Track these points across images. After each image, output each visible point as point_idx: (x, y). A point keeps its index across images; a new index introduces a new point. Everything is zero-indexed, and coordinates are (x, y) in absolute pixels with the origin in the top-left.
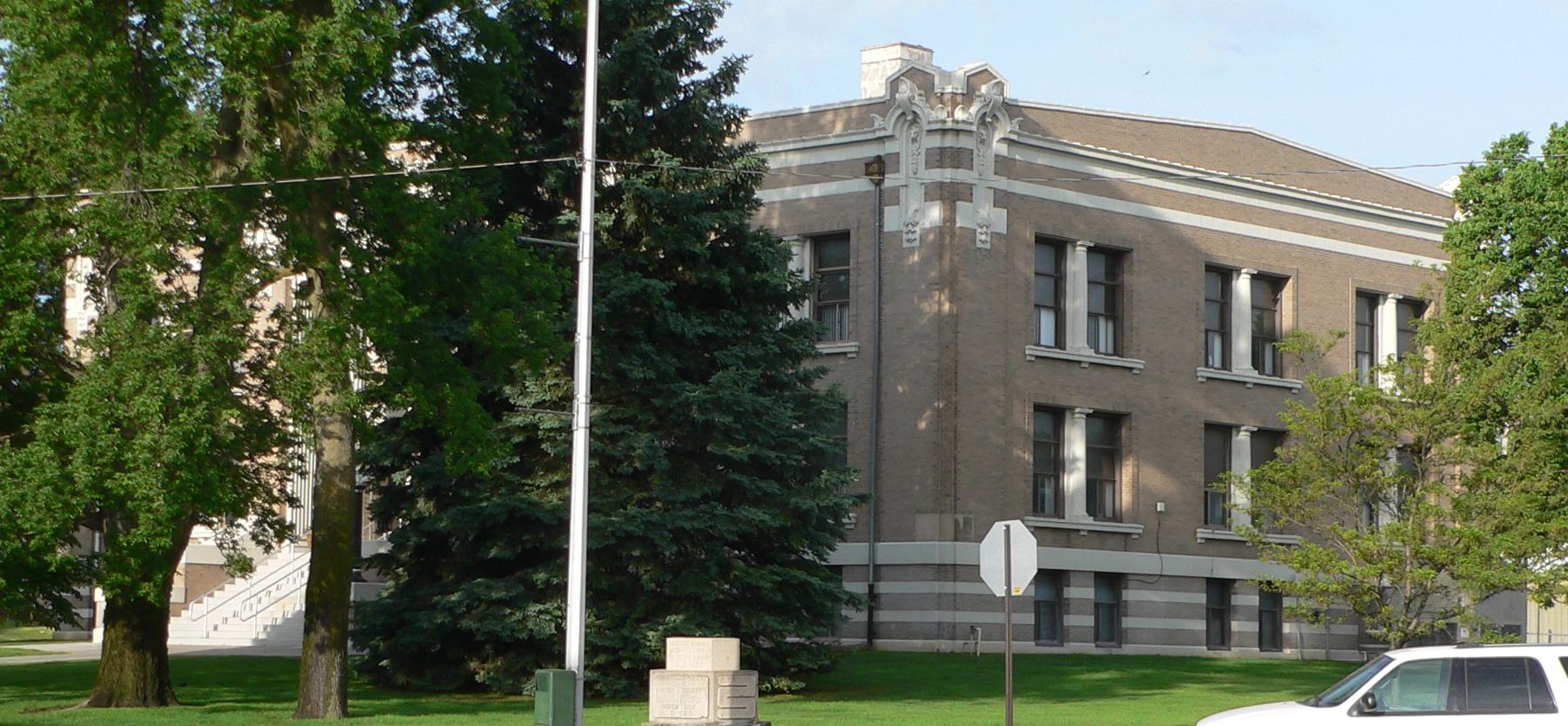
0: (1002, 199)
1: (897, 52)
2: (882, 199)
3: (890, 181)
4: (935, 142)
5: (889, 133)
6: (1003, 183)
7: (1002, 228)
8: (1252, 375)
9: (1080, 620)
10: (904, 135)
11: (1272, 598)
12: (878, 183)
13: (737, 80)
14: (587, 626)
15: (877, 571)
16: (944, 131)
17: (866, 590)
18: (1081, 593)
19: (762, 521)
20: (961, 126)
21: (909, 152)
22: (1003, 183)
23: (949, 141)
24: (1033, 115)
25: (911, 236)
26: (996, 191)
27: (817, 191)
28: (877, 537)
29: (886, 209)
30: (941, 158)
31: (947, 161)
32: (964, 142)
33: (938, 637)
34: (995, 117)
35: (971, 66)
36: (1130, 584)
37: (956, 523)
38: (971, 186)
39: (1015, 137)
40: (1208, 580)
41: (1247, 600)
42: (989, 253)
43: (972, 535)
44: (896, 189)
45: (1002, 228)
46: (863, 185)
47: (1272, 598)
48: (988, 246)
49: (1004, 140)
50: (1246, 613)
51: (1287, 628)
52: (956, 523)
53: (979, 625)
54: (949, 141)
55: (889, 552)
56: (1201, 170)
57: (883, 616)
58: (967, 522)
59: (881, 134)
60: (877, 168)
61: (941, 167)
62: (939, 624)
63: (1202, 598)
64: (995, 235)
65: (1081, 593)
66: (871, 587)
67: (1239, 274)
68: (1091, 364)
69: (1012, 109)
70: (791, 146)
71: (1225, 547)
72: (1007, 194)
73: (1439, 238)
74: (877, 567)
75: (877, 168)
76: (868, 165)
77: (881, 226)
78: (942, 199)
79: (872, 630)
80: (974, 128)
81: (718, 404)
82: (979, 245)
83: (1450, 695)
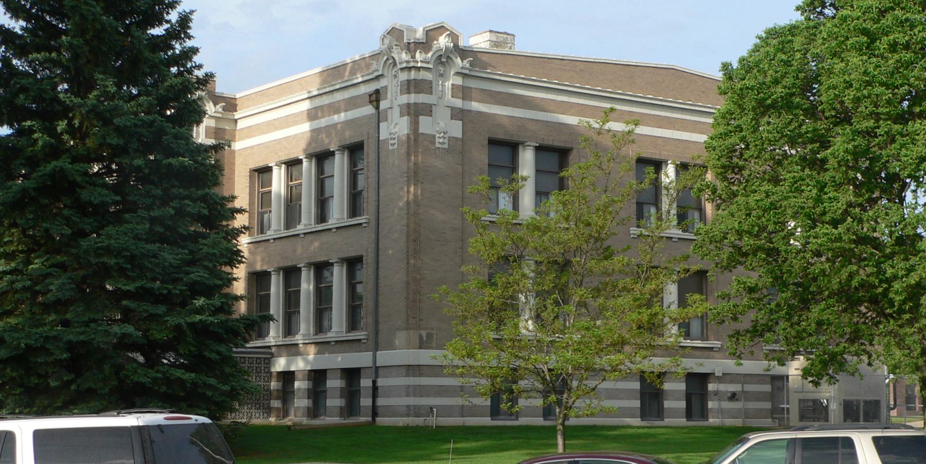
0: (458, 114)
1: (487, 36)
2: (379, 117)
3: (383, 105)
4: (404, 76)
5: (380, 73)
7: (459, 134)
8: (676, 232)
9: (334, 402)
10: (389, 73)
11: (698, 383)
12: (377, 108)
13: (189, 28)
14: (21, 413)
15: (377, 370)
16: (410, 69)
17: (371, 385)
18: (334, 383)
19: (124, 335)
21: (391, 83)
23: (413, 74)
24: (485, 58)
25: (392, 142)
27: (342, 117)
28: (376, 348)
29: (381, 124)
30: (411, 86)
31: (412, 89)
32: (428, 76)
33: (408, 415)
35: (430, 24)
36: (711, 380)
37: (421, 337)
38: (431, 106)
39: (467, 72)
40: (342, 369)
41: (675, 386)
43: (434, 344)
44: (386, 110)
45: (459, 134)
46: (369, 110)
47: (698, 383)
48: (446, 146)
49: (458, 74)
50: (674, 395)
51: (710, 405)
52: (421, 337)
53: (436, 406)
54: (413, 74)
55: (385, 357)
56: (649, 98)
57: (380, 402)
58: (429, 336)
59: (376, 74)
60: (376, 98)
61: (409, 93)
62: (408, 406)
63: (637, 385)
65: (334, 383)
66: (374, 382)
67: (667, 165)
68: (679, 239)
69: (464, 53)
70: (338, 87)
73: (711, 121)
74: (377, 368)
75: (376, 98)
76: (370, 96)
78: (409, 114)
79: (375, 412)
81: (108, 251)
82: (437, 145)
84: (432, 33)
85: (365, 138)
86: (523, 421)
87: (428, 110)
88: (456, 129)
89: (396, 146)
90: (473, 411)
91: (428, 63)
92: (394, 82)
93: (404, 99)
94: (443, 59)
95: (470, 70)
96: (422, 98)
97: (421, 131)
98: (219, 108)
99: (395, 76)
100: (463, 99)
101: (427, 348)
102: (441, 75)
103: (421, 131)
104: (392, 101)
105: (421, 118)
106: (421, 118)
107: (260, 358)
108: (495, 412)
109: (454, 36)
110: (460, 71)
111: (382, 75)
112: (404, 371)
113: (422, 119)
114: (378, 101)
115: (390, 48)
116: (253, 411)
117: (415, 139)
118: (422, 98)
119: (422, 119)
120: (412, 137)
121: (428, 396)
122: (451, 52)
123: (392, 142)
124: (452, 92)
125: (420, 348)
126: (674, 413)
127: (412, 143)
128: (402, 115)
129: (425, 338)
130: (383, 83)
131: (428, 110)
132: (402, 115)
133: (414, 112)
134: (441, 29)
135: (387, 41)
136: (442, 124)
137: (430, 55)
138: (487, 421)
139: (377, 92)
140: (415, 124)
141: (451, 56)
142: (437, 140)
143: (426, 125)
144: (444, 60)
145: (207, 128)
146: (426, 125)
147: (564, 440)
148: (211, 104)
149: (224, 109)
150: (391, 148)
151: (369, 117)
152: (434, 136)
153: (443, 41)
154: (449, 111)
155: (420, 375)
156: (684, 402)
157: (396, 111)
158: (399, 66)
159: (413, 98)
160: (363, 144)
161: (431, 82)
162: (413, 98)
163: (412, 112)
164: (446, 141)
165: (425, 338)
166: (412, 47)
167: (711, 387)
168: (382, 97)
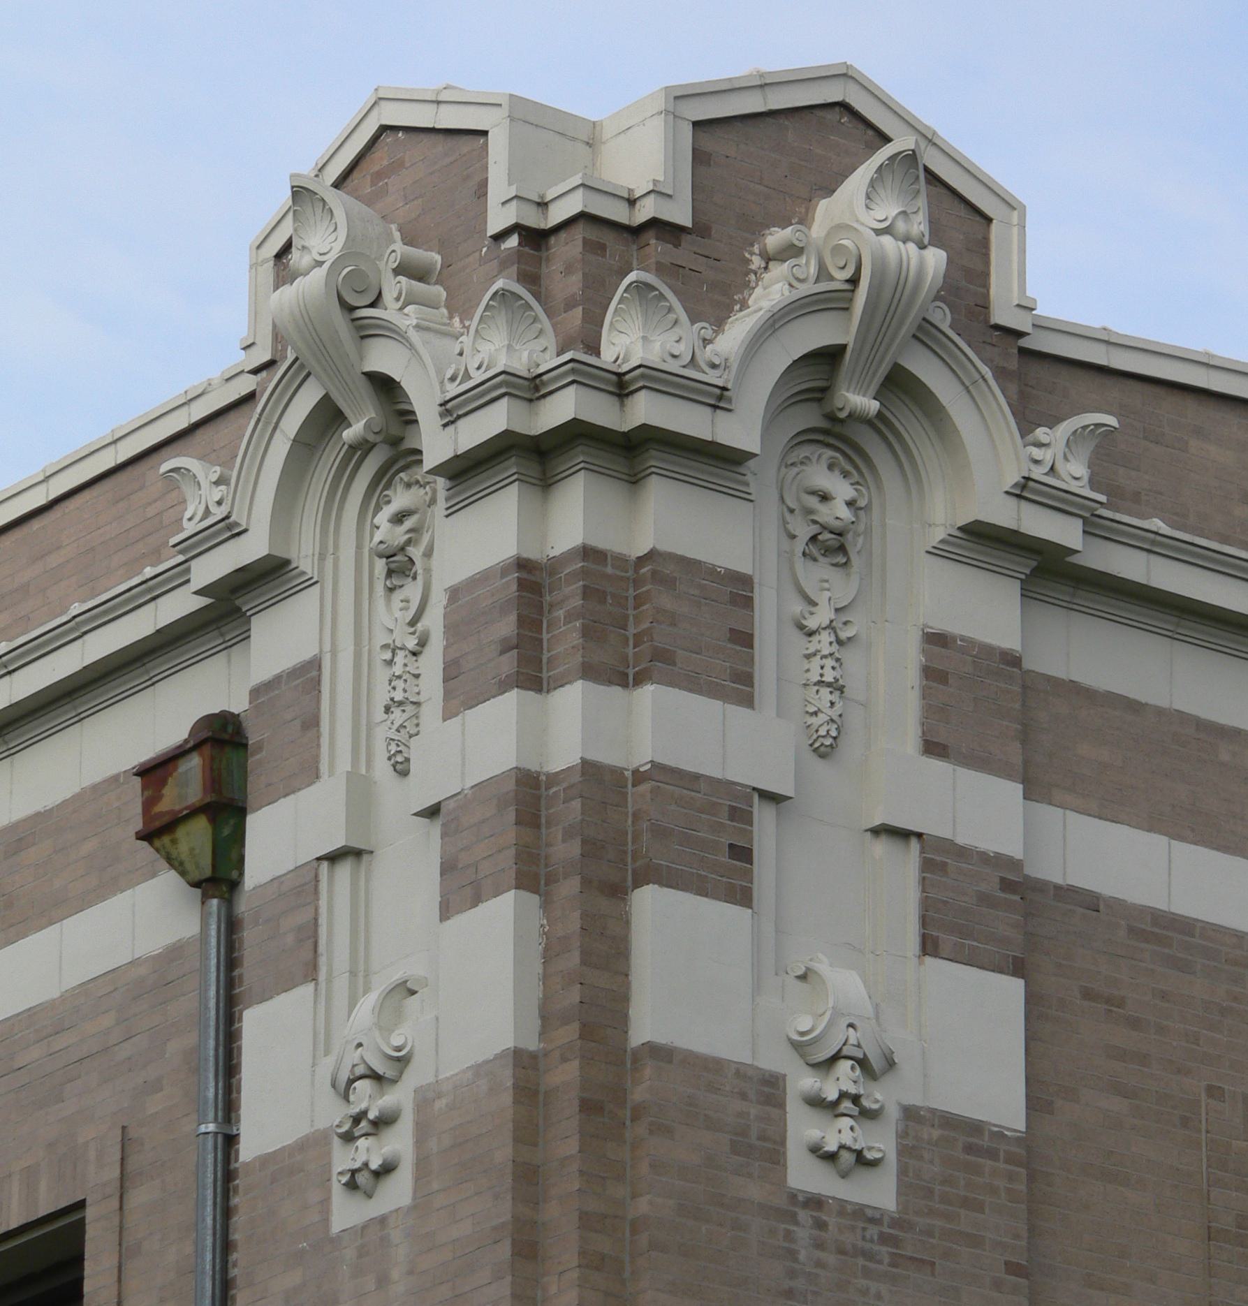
0: (981, 912)
3: (277, 839)
4: (482, 538)
5: (251, 549)
6: (986, 812)
7: (992, 1091)
12: (220, 880)
20: (645, 410)
22: (986, 812)
25: (370, 1152)
26: (939, 858)
29: (252, 1021)
30: (544, 625)
31: (564, 639)
34: (899, 384)
39: (1061, 531)
42: (884, 1242)
45: (992, 1091)
46: (151, 915)
48: (880, 1192)
49: (984, 541)
54: (575, 516)
61: (533, 675)
64: (945, 1142)
69: (1039, 372)
71: (1140, 346)
72: (1016, 885)
75: (201, 803)
77: (230, 1141)
78: (531, 876)
80: (740, 430)
82: (805, 1176)
83: (510, 323)
85: (95, 1180)
87: (713, 839)
88: (969, 1046)
89: (397, 1193)
91: (719, 400)
92: (389, 617)
93: (490, 740)
94: (853, 402)
95: (1093, 527)
96: (658, 726)
97: (649, 1022)
99: (398, 565)
100: (1034, 790)
102: (832, 546)
104: (360, 794)
105: (649, 903)
106: (649, 903)
109: (963, 216)
110: (1004, 514)
111: (253, 344)
112: (1025, 566)
113: (656, 912)
114: (227, 812)
115: (355, 307)
117: (590, 1086)
118: (658, 726)
119: (656, 912)
120: (565, 1076)
122: (925, 334)
123: (370, 1152)
124: (933, 711)
127: (564, 1141)
128: (460, 889)
130: (280, 638)
131: (713, 839)
132: (460, 889)
133: (585, 853)
135: (323, 243)
136: (846, 985)
137: (737, 333)
139: (221, 737)
140: (588, 979)
141: (926, 369)
142: (804, 1128)
143: (693, 974)
144: (858, 399)
146: (693, 974)
150: (346, 1213)
151: (149, 981)
152: (770, 1089)
154: (899, 878)
157: (409, 864)
158: (438, 444)
159: (572, 725)
160: (78, 1229)
161: (738, 590)
162: (572, 725)
163: (564, 850)
164: (881, 1141)
166: (578, 253)
168: (261, 769)
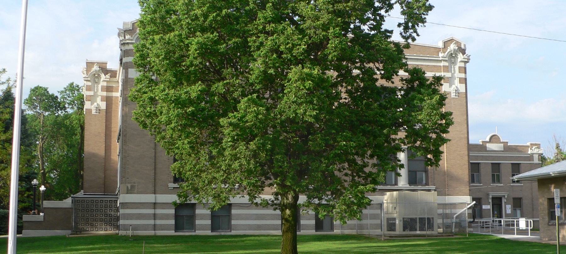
43: (136, 191)
50: (203, 217)
84: (446, 43)
86: (198, 233)
90: (163, 227)
97: (129, 77)
98: (108, 76)
101: (131, 193)
103: (129, 77)
107: (84, 200)
108: (177, 227)
109: (458, 43)
116: (108, 227)
121: (131, 219)
125: (127, 193)
126: (203, 227)
129: (130, 188)
134: (451, 40)
138: (172, 233)
145: (459, 67)
147: (501, 233)
148: (461, 54)
149: (111, 77)
153: (452, 47)
155: (128, 208)
156: (210, 221)
165: (130, 188)
167: (234, 212)
